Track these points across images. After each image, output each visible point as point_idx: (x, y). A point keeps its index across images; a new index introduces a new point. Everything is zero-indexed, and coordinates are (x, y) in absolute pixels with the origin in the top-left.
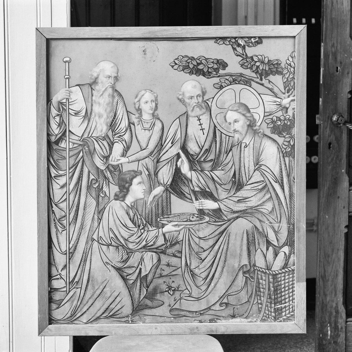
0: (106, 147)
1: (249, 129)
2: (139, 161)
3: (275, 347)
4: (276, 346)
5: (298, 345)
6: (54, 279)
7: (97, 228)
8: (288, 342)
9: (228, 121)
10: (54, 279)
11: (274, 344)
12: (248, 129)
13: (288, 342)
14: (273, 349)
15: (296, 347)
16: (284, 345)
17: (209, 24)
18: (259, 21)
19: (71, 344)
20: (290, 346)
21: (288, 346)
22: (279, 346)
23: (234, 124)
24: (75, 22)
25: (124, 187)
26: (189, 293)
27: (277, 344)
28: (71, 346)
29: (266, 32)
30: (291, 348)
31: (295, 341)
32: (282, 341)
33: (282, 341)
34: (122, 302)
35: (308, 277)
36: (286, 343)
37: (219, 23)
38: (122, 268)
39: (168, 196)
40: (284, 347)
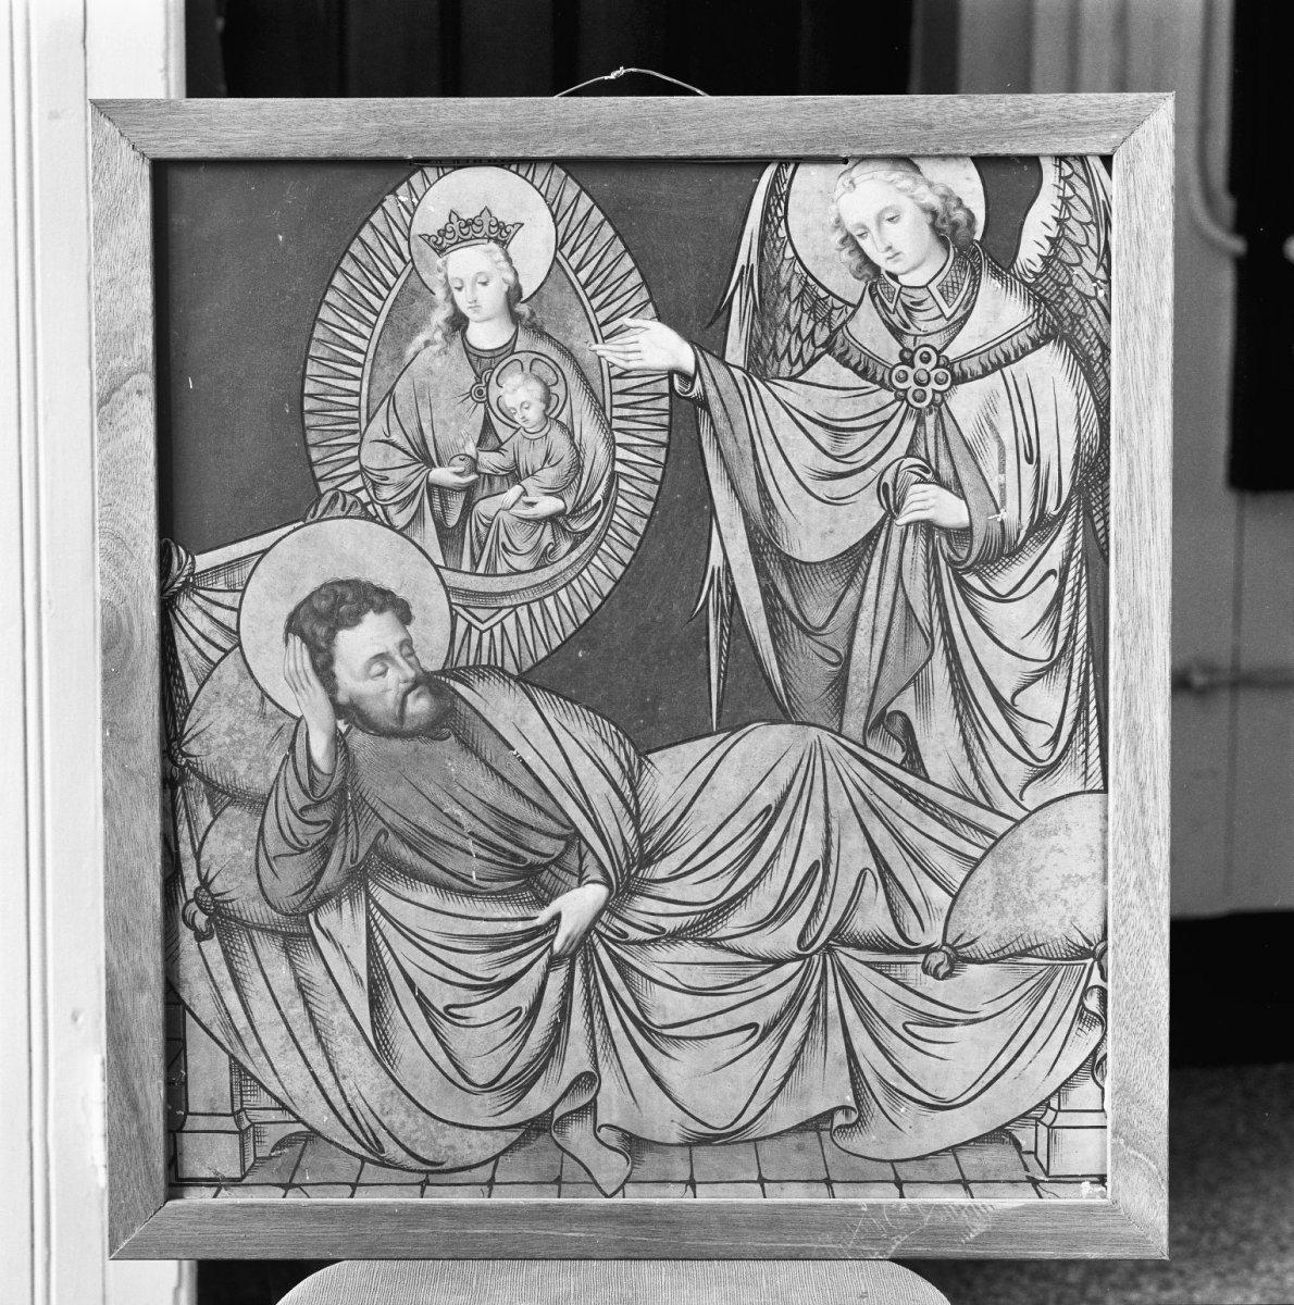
1: (1247, 521)
2: (955, 897)
3: (1205, 1241)
4: (1212, 1241)
8: (1267, 1220)
11: (1202, 1231)
12: (1240, 520)
14: (1194, 1254)
16: (1246, 1236)
17: (895, 83)
18: (1086, 74)
19: (172, 35)
20: (1276, 1239)
21: (1266, 1239)
22: (1225, 1238)
24: (197, 86)
27: (1214, 1230)
28: (172, 42)
30: (1283, 1249)
32: (1236, 1215)
34: (426, 567)
35: (1179, 911)
36: (1257, 1225)
37: (944, 81)
38: (657, 1033)
39: (892, 782)
40: (1247, 1247)
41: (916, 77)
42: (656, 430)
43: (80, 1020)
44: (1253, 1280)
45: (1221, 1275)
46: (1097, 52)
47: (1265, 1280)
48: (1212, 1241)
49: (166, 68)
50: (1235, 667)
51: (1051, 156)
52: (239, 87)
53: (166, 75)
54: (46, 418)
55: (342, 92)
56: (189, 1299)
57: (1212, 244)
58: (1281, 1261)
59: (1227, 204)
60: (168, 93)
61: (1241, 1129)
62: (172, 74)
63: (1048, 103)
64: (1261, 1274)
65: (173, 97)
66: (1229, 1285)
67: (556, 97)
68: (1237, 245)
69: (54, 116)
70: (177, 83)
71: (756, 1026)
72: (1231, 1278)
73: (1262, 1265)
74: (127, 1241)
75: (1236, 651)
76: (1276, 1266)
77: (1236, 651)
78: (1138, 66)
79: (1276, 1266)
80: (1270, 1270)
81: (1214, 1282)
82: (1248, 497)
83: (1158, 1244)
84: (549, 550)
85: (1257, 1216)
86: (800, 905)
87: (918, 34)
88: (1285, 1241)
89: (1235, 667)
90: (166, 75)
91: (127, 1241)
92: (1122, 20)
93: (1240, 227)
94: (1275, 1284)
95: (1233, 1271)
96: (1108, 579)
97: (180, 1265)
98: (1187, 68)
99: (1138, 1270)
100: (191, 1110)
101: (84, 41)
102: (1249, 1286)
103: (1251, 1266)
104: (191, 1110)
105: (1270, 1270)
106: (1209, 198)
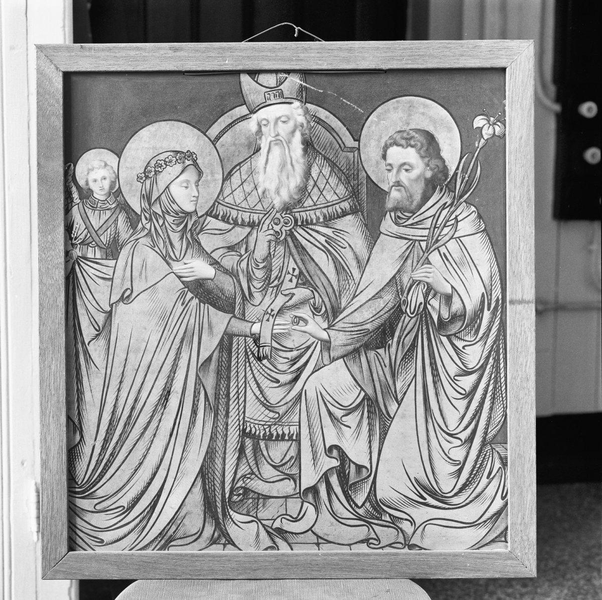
0: (250, 372)
4: (546, 565)
5: (592, 563)
6: (430, 300)
7: (352, 323)
8: (571, 555)
9: (389, 161)
10: (430, 300)
13: (571, 555)
15: (590, 567)
16: (562, 563)
18: (487, 31)
19: (67, 14)
21: (571, 564)
23: (399, 171)
24: (79, 36)
25: (42, 74)
26: (283, 519)
29: (523, 138)
30: (578, 569)
31: (587, 553)
32: (556, 553)
33: (556, 553)
35: (548, 412)
36: (566, 558)
37: (422, 34)
40: (562, 568)
41: (409, 32)
42: (159, 254)
43: (25, 465)
44: (565, 583)
45: (550, 581)
46: (492, 18)
47: (570, 583)
48: (546, 565)
49: (64, 26)
50: (556, 302)
51: (196, 209)
52: (98, 38)
53: (64, 30)
54: (9, 188)
55: (145, 38)
56: (75, 595)
57: (545, 107)
58: (577, 574)
59: (552, 89)
60: (65, 41)
61: (559, 514)
62: (67, 29)
63: (467, 44)
64: (568, 580)
65: (67, 43)
66: (553, 585)
67: (243, 42)
68: (557, 108)
69: (12, 48)
70: (69, 33)
71: (500, 468)
72: (554, 582)
73: (568, 576)
74: (51, 570)
75: (557, 297)
76: (576, 577)
77: (557, 297)
78: (512, 26)
79: (576, 577)
80: (572, 578)
81: (547, 584)
82: (562, 223)
83: (530, 568)
84: (126, 295)
85: (567, 554)
86: (131, 430)
87: (410, 11)
88: (579, 565)
89: (556, 302)
90: (64, 30)
91: (51, 570)
92: (503, 8)
93: (558, 99)
94: (575, 585)
95: (556, 579)
96: (506, 259)
97: (71, 582)
98: (535, 27)
99: (524, 582)
100: (270, 526)
101: (26, 14)
102: (563, 586)
103: (563, 576)
104: (270, 526)
105: (572, 578)
106: (544, 86)
